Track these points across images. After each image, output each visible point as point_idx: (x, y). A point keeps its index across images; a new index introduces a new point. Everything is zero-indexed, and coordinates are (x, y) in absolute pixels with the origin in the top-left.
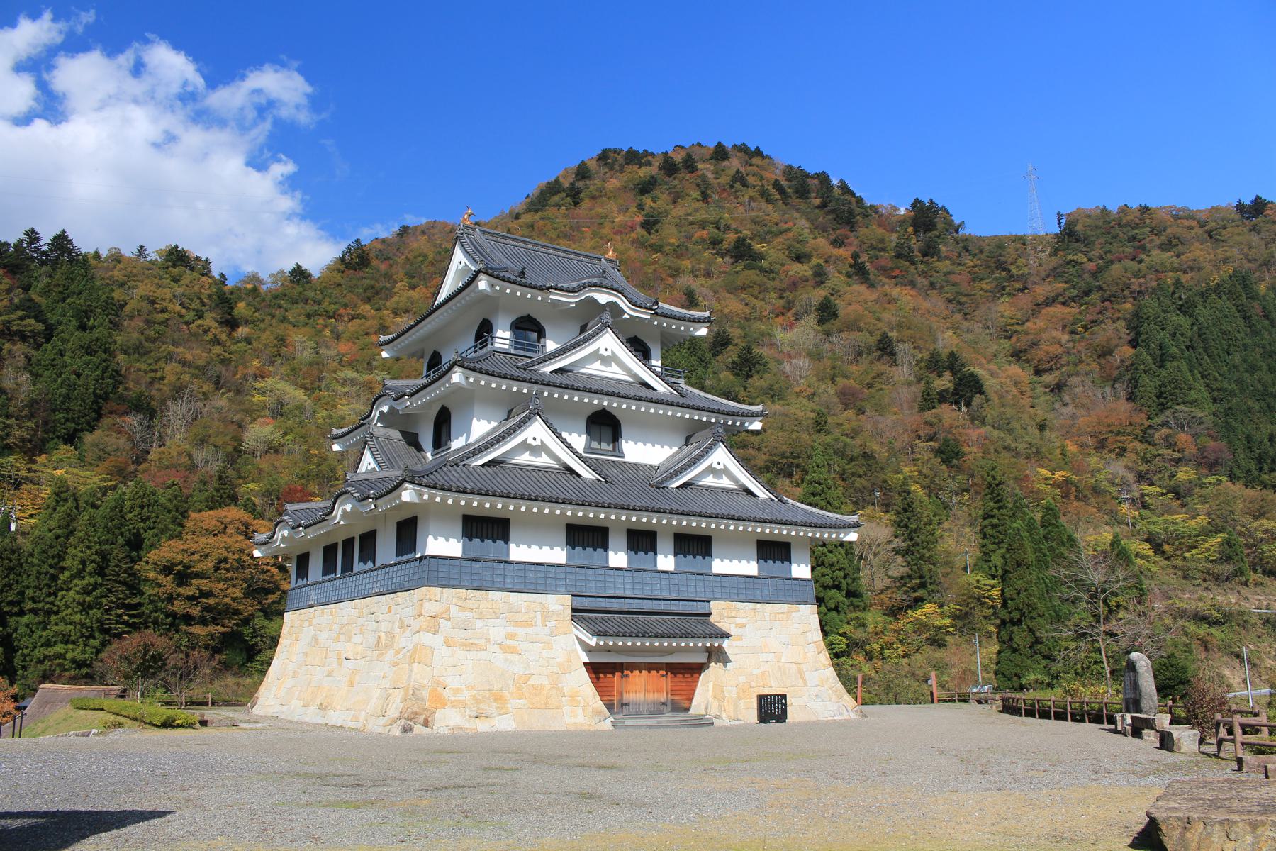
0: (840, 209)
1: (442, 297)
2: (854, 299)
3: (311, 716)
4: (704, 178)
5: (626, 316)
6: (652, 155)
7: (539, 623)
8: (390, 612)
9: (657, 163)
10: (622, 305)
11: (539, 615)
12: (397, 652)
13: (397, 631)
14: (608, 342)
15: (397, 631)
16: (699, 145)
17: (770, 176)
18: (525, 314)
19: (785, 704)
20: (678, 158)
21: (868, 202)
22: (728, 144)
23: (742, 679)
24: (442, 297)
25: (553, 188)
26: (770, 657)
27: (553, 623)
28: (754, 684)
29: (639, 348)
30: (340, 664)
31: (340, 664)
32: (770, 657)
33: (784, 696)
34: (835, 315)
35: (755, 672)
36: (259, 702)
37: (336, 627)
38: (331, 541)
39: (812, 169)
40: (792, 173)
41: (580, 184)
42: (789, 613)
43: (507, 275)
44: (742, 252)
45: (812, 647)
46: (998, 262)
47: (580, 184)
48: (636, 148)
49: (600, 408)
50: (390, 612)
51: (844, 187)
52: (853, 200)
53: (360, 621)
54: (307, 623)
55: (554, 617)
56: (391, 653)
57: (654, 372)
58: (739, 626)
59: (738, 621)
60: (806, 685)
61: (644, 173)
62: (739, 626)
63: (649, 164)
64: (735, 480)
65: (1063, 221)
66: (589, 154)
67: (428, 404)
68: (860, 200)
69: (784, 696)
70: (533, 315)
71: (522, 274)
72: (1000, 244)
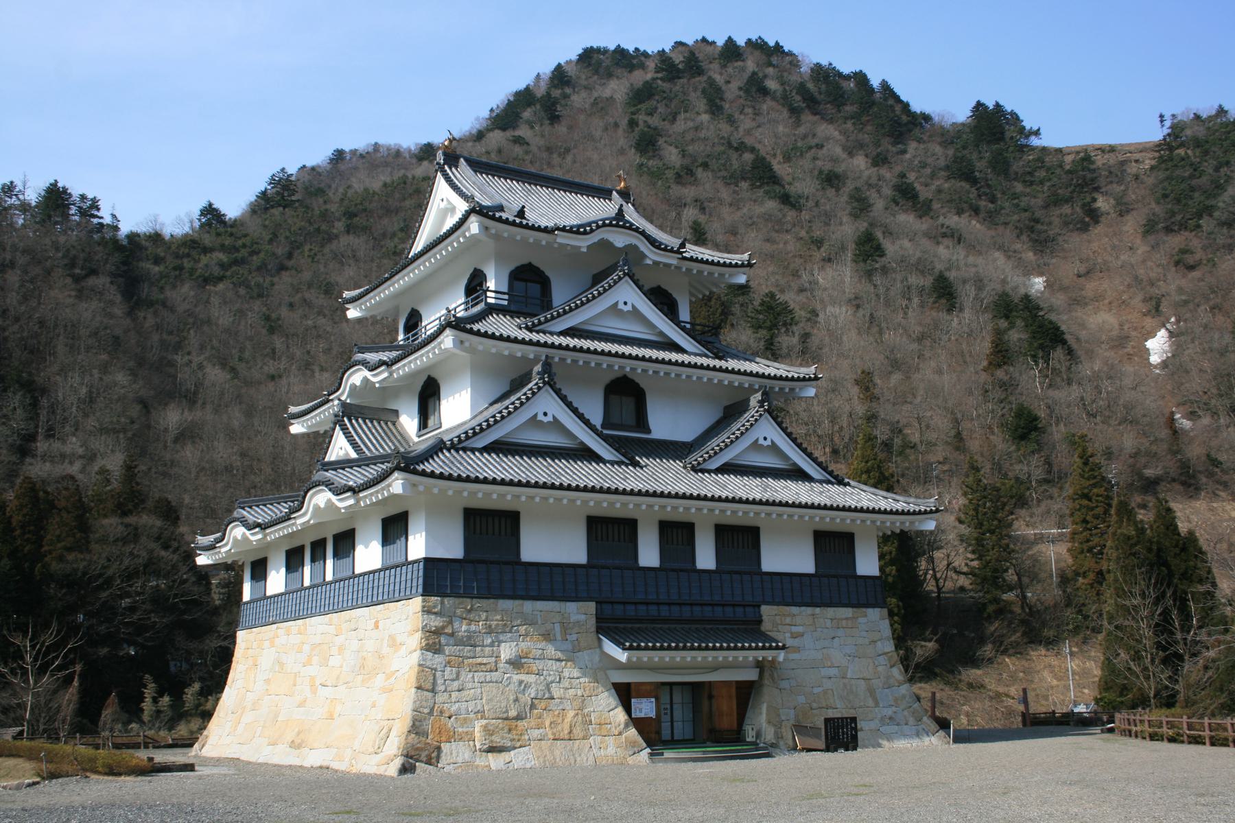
0: (875, 112)
1: (418, 246)
2: (907, 238)
3: (280, 756)
4: (712, 82)
5: (649, 262)
6: (645, 54)
7: (559, 637)
8: (377, 627)
9: (651, 65)
10: (643, 248)
11: (557, 627)
12: (388, 677)
13: (386, 650)
14: (627, 295)
15: (386, 650)
16: (704, 40)
17: (794, 78)
18: (525, 261)
19: (855, 729)
20: (678, 59)
21: (916, 107)
22: (741, 42)
23: (801, 699)
24: (418, 246)
25: (524, 98)
26: (833, 672)
27: (574, 637)
28: (815, 705)
29: (663, 300)
30: (314, 692)
31: (314, 692)
32: (833, 672)
33: (854, 720)
34: (882, 255)
35: (816, 690)
36: (210, 742)
37: (306, 648)
38: (296, 543)
39: (846, 69)
40: (825, 74)
41: (556, 93)
42: (854, 618)
43: (504, 216)
44: (762, 175)
45: (882, 660)
46: (1082, 179)
47: (556, 93)
48: (624, 46)
49: (619, 375)
50: (376, 626)
51: (885, 86)
52: (898, 108)
53: (339, 640)
54: (267, 644)
55: (575, 630)
56: (381, 677)
57: (683, 329)
58: (794, 636)
59: (794, 629)
60: (877, 705)
61: (639, 77)
62: (794, 636)
63: (642, 66)
64: (785, 457)
65: (1168, 123)
66: (568, 52)
67: (413, 375)
68: (906, 106)
69: (854, 720)
70: (535, 263)
71: (521, 214)
72: (1085, 157)
